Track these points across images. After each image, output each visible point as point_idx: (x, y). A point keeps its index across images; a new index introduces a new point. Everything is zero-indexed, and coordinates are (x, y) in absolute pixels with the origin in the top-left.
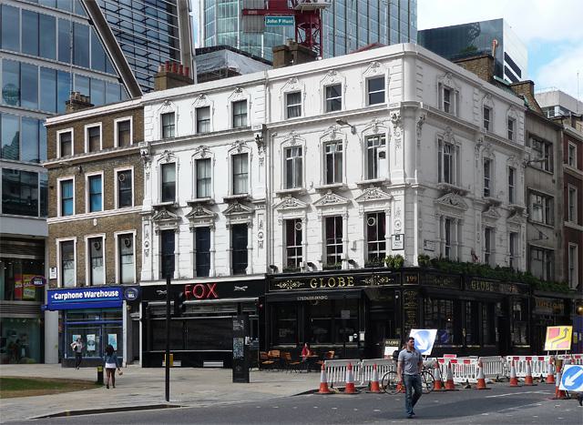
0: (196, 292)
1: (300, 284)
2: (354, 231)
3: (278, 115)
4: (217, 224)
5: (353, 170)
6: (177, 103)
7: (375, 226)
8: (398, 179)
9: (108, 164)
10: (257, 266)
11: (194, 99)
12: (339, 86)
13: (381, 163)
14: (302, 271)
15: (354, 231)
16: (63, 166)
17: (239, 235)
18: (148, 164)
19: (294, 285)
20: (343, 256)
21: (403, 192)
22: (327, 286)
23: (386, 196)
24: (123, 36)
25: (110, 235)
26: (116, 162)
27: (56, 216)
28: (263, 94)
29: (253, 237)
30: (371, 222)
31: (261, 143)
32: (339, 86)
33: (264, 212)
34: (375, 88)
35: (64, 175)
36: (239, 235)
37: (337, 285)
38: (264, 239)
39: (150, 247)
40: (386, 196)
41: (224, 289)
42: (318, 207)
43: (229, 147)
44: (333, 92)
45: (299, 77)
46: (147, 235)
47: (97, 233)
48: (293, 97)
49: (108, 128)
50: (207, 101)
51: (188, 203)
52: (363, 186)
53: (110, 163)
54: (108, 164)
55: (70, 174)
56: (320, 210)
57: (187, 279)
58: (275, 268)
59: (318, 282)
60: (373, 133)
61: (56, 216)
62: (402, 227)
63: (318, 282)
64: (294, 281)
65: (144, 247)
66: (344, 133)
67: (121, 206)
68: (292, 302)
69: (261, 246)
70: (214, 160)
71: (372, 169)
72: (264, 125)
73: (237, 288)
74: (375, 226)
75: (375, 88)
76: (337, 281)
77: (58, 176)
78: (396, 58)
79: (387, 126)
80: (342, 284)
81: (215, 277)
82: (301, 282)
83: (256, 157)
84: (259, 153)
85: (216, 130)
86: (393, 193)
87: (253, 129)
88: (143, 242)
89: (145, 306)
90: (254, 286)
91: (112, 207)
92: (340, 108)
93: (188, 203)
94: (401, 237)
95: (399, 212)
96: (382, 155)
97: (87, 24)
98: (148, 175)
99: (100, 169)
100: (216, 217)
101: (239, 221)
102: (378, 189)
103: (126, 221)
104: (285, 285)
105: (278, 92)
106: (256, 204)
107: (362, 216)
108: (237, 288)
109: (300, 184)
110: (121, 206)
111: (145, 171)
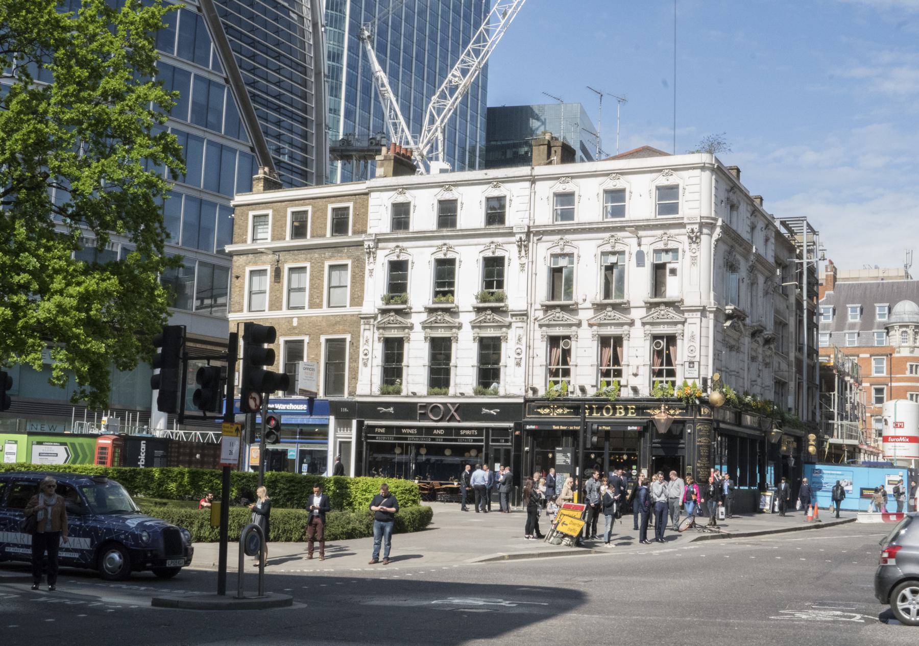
0: (431, 411)
1: (566, 411)
2: (637, 354)
3: (544, 216)
4: (413, 336)
5: (637, 284)
6: (461, 189)
7: (663, 349)
8: (691, 300)
9: (316, 256)
10: (513, 384)
11: (438, 190)
12: (623, 191)
13: (670, 281)
14: (570, 396)
15: (637, 354)
16: (255, 252)
17: (489, 349)
18: (371, 259)
19: (560, 411)
20: (623, 382)
21: (699, 314)
22: (602, 414)
23: (678, 318)
24: (257, 98)
25: (315, 338)
26: (328, 253)
27: (241, 310)
28: (527, 192)
29: (508, 352)
30: (658, 344)
31: (523, 245)
32: (623, 191)
33: (524, 325)
34: (668, 197)
35: (255, 263)
36: (489, 349)
37: (614, 413)
38: (523, 356)
39: (369, 356)
40: (678, 318)
41: (468, 411)
42: (591, 325)
43: (482, 248)
44: (616, 196)
45: (573, 177)
46: (367, 341)
47: (298, 334)
48: (566, 198)
49: (320, 213)
50: (503, 190)
51: (426, 308)
52: (431, 311)
53: (320, 254)
54: (316, 256)
55: (264, 263)
56: (381, 331)
57: (420, 397)
58: (535, 391)
59: (591, 409)
60: (663, 247)
61: (241, 310)
62: (697, 354)
63: (591, 409)
64: (562, 407)
65: (361, 356)
66: (629, 244)
67: (271, 309)
68: (549, 431)
69: (518, 364)
70: (413, 263)
71: (658, 285)
72: (529, 227)
73: (485, 411)
74: (663, 349)
75: (668, 197)
76: (615, 409)
77: (247, 264)
78: (694, 168)
79: (680, 240)
80: (620, 413)
81: (455, 396)
82: (568, 408)
83: (688, 254)
84: (520, 258)
85: (463, 228)
86: (686, 315)
87: (515, 231)
88: (361, 350)
89: (360, 424)
90: (508, 410)
91: (319, 306)
92: (623, 215)
93: (426, 308)
94: (696, 365)
95: (693, 337)
96: (673, 272)
97: (222, 82)
98: (371, 271)
99: (306, 260)
100: (411, 328)
101: (440, 333)
102: (671, 309)
103: (337, 323)
104: (547, 411)
105: (545, 190)
106: (513, 315)
107: (596, 338)
108: (485, 411)
109: (569, 294)
110: (271, 309)
111: (367, 267)
